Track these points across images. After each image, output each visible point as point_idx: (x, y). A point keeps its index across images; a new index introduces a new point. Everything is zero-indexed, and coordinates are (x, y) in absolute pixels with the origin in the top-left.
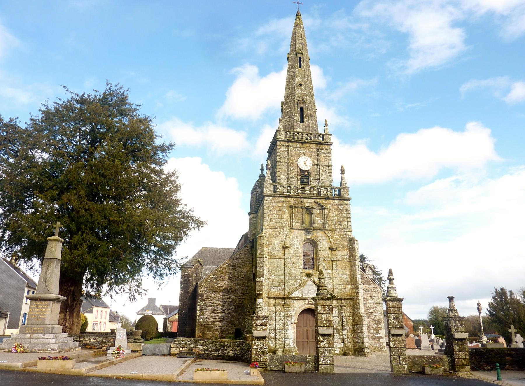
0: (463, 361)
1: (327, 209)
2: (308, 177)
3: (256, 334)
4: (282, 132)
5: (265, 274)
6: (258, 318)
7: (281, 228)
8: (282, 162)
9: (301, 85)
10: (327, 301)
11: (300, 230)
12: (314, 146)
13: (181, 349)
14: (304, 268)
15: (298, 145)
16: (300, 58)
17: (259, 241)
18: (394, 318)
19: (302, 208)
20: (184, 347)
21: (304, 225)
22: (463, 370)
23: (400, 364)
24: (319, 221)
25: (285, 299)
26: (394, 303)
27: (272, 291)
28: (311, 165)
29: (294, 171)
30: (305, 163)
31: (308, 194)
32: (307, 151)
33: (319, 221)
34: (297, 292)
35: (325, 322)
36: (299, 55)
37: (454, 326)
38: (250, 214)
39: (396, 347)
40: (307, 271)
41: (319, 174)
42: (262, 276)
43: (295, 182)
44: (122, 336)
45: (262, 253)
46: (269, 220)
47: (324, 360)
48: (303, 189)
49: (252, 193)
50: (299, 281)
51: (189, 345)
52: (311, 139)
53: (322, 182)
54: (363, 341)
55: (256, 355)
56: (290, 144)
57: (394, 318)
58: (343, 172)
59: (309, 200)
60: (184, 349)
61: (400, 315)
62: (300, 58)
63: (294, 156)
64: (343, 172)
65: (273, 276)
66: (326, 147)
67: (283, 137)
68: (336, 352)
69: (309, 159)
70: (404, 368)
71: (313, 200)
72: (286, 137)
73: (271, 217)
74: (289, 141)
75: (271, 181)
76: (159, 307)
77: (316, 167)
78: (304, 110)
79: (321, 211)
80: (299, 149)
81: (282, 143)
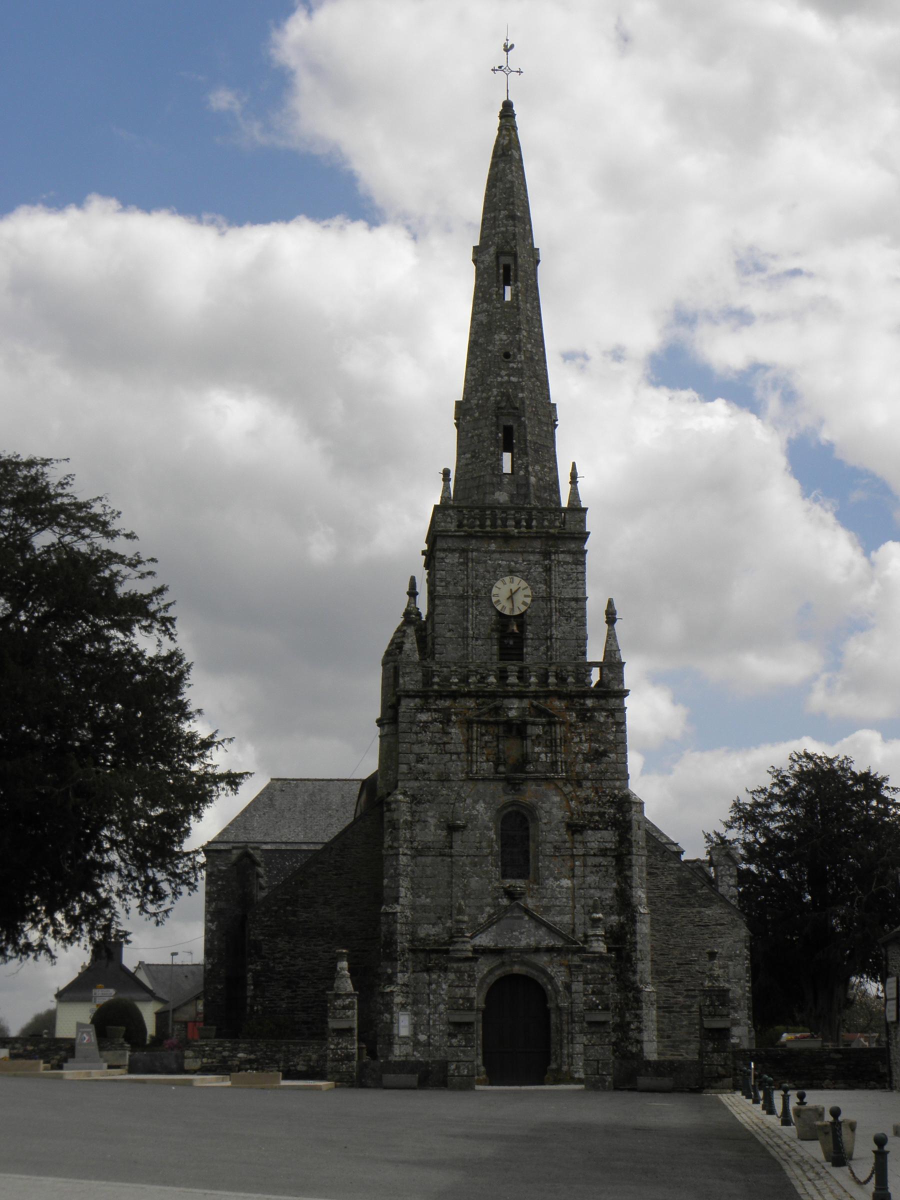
0: (720, 1069)
1: (562, 723)
2: (520, 639)
3: (333, 1024)
4: (451, 512)
5: (402, 894)
6: (338, 996)
7: (444, 779)
8: (450, 597)
9: (507, 355)
10: (467, 964)
11: (493, 780)
12: (537, 545)
13: (205, 1060)
14: (504, 876)
15: (493, 547)
16: (507, 268)
17: (388, 814)
18: (593, 993)
19: (497, 723)
20: (210, 1056)
21: (502, 769)
22: (720, 1084)
23: (598, 1074)
24: (543, 756)
25: (435, 956)
26: (595, 965)
27: (422, 932)
28: (528, 600)
29: (489, 619)
30: (511, 594)
31: (513, 685)
32: (520, 562)
33: (543, 756)
34: (483, 936)
35: (461, 1001)
36: (505, 260)
37: (708, 1006)
38: (380, 723)
39: (593, 1045)
40: (508, 882)
41: (549, 625)
42: (396, 900)
43: (484, 652)
44: (87, 1038)
45: (396, 845)
46: (412, 757)
47: (458, 1068)
48: (502, 676)
49: (384, 664)
50: (488, 909)
51: (221, 1052)
52: (529, 526)
53: (557, 645)
54: (642, 1049)
55: (333, 1060)
56: (473, 544)
57: (593, 993)
58: (611, 617)
59: (515, 703)
60: (210, 1061)
61: (605, 987)
62: (507, 268)
63: (484, 578)
64: (611, 617)
65: (424, 900)
66: (573, 546)
67: (452, 527)
68: (576, 1076)
69: (524, 584)
70: (605, 1081)
71: (526, 703)
72: (460, 525)
73: (416, 748)
74: (470, 536)
75: (417, 657)
76: (132, 970)
77: (542, 604)
78: (516, 434)
79: (547, 728)
80: (497, 556)
81: (450, 543)
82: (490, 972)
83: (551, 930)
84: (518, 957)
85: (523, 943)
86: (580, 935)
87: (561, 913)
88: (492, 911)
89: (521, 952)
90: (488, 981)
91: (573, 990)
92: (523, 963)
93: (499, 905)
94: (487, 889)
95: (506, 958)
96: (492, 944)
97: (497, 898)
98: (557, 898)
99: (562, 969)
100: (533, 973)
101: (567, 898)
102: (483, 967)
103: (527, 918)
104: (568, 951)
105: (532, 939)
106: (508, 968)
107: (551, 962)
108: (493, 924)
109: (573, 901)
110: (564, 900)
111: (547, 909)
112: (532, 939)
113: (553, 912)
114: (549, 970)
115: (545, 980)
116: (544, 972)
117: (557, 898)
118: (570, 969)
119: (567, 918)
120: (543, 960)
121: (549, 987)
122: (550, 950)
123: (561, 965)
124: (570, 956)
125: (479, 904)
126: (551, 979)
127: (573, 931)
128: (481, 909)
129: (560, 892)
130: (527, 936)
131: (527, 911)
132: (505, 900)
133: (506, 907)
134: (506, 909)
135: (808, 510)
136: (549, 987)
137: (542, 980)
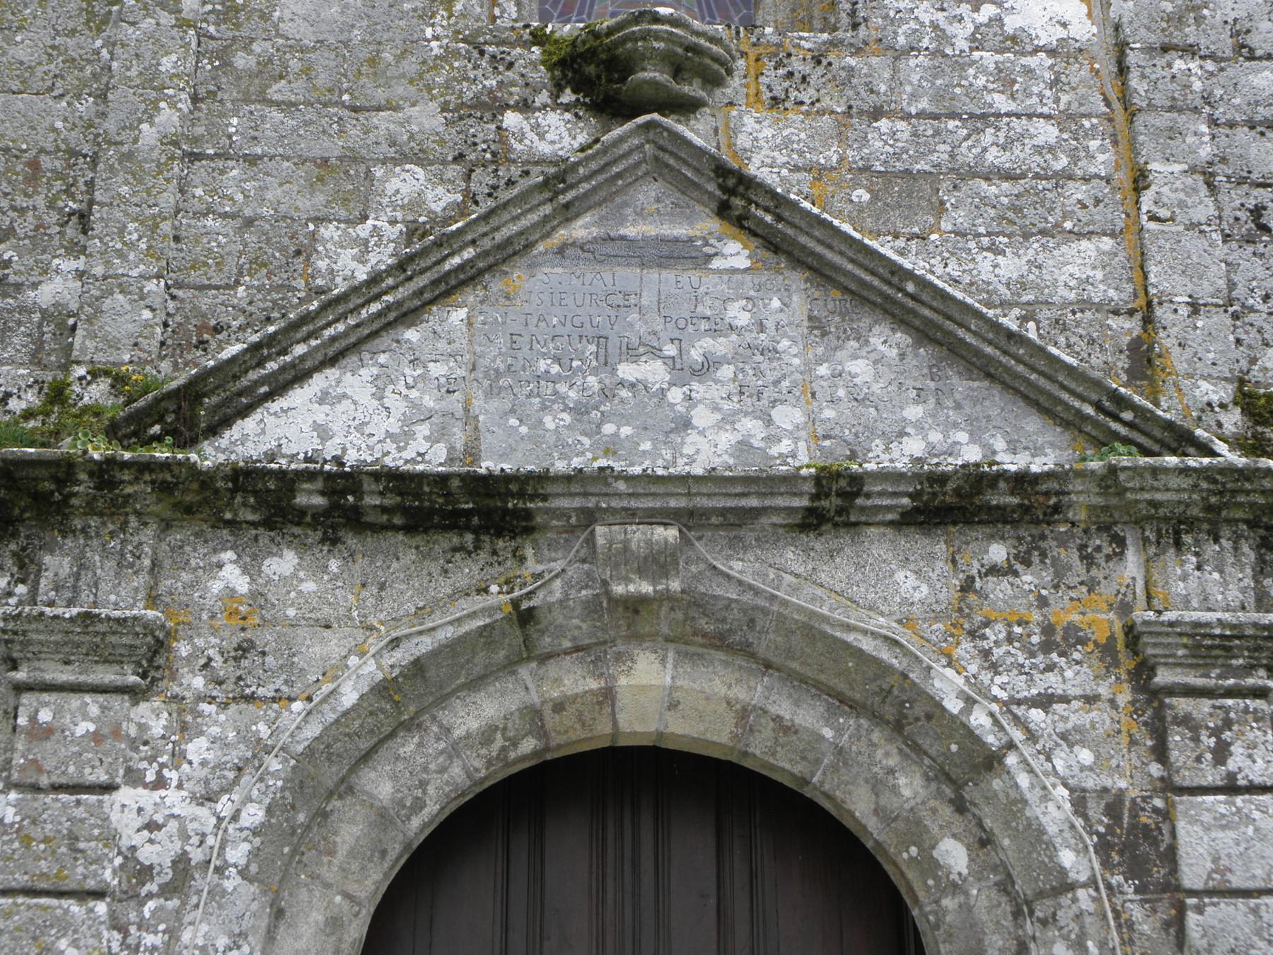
34: (354, 381)
82: (407, 698)
83: (944, 332)
84: (658, 563)
85: (708, 448)
86: (1211, 392)
87: (1017, 226)
88: (440, 199)
89: (690, 519)
90: (380, 784)
91: (1193, 874)
92: (717, 633)
93: (500, 156)
94: (412, 43)
95: (550, 573)
96: (428, 453)
97: (492, 106)
98: (984, 119)
99: (1073, 676)
100: (797, 735)
101: (1066, 119)
102: (334, 645)
103: (735, 254)
104: (1125, 517)
105: (788, 416)
106: (573, 680)
107: (965, 615)
108: (447, 289)
109: (1125, 142)
110: (1047, 132)
111: (906, 189)
112: (788, 416)
113: (959, 217)
114: (947, 687)
115: (910, 786)
116: (897, 707)
117: (984, 119)
118: (1142, 674)
119: (1080, 267)
120: (886, 591)
121: (954, 855)
122: (946, 505)
123: (1058, 641)
124: (1132, 566)
125: (333, 147)
126: (966, 769)
127: (1143, 360)
128: (346, 180)
129: (1005, 80)
130: (719, 379)
131: (734, 195)
132: (554, 121)
133: (559, 177)
134: (558, 185)
135: (1074, 439)
136: (954, 855)
137: (877, 790)
